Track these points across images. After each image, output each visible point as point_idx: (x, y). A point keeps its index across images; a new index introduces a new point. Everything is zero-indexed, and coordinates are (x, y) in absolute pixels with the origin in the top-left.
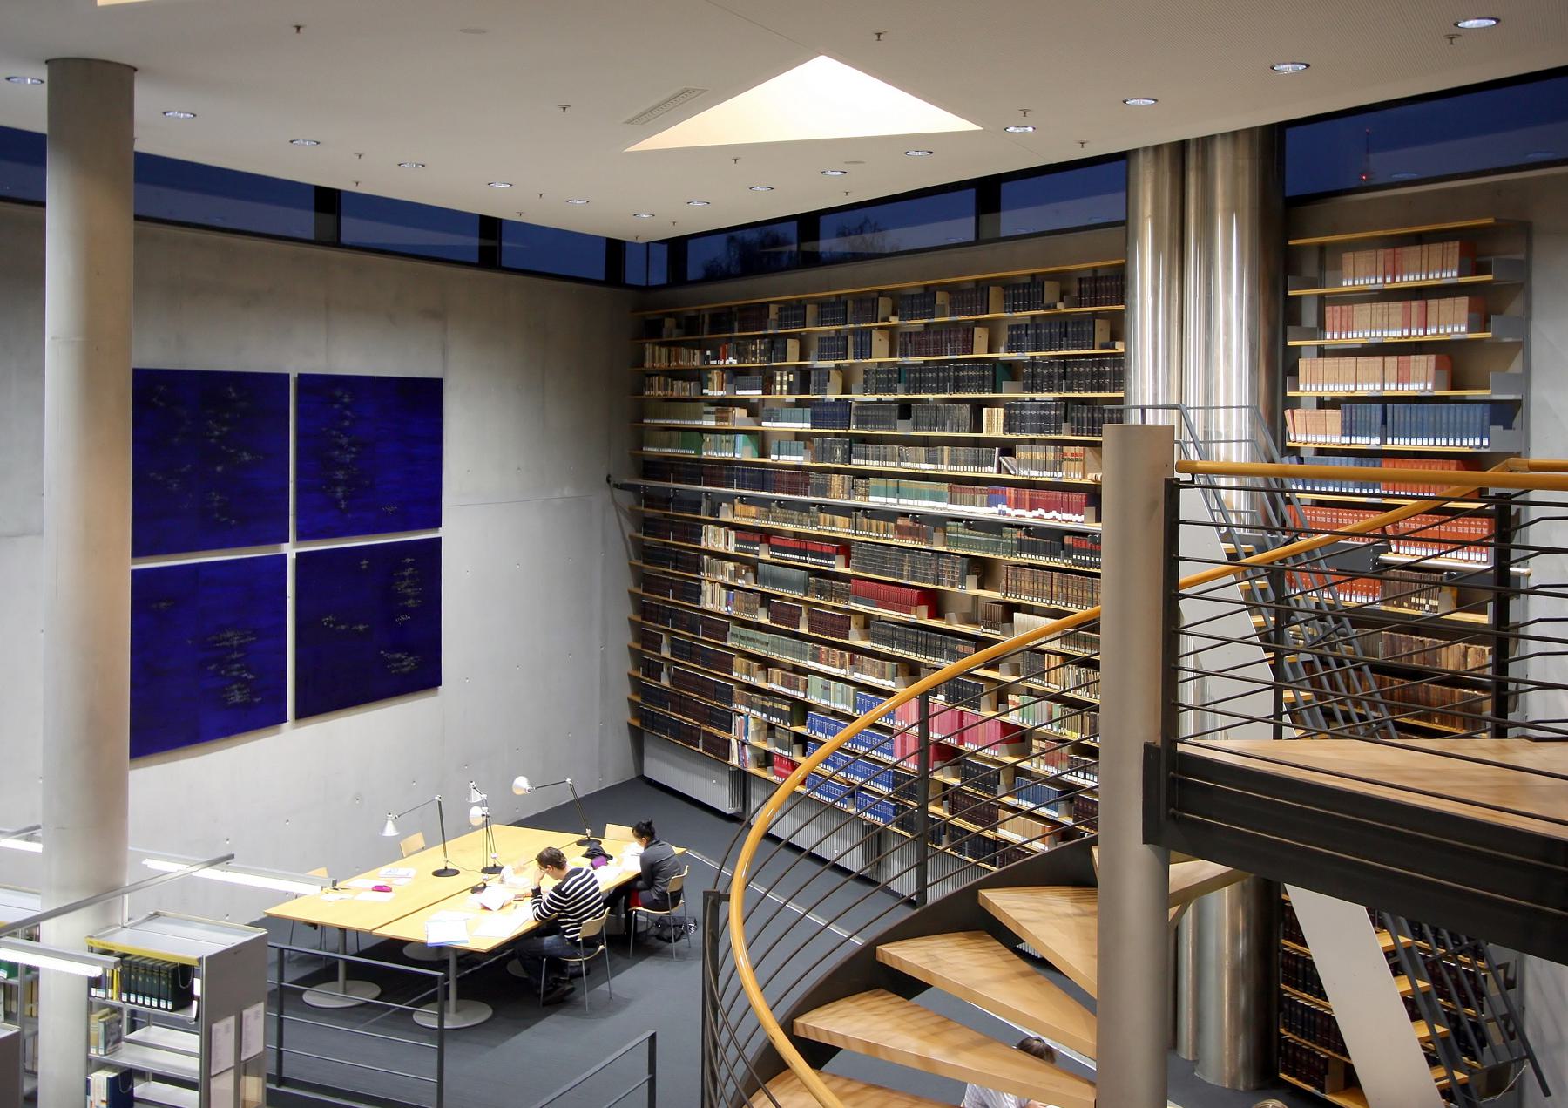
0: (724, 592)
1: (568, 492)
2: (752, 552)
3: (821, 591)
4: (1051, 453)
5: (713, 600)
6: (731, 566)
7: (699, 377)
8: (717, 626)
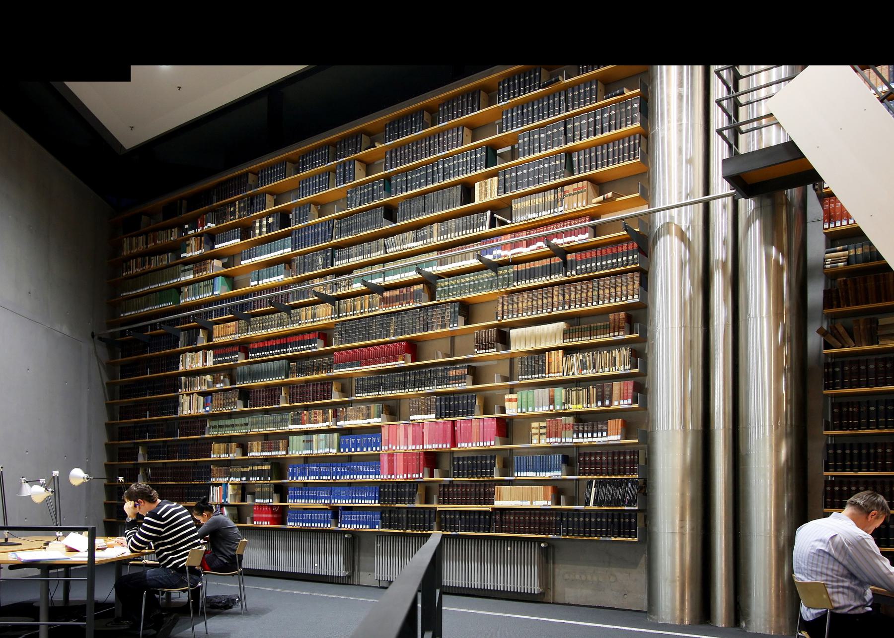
0: (201, 399)
1: (65, 330)
2: (231, 360)
3: (301, 371)
4: (550, 196)
5: (190, 406)
6: (208, 378)
7: (178, 248)
8: (197, 423)
